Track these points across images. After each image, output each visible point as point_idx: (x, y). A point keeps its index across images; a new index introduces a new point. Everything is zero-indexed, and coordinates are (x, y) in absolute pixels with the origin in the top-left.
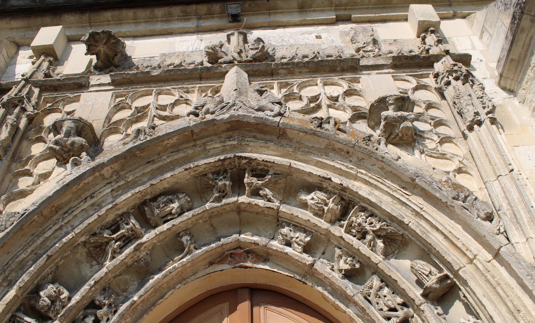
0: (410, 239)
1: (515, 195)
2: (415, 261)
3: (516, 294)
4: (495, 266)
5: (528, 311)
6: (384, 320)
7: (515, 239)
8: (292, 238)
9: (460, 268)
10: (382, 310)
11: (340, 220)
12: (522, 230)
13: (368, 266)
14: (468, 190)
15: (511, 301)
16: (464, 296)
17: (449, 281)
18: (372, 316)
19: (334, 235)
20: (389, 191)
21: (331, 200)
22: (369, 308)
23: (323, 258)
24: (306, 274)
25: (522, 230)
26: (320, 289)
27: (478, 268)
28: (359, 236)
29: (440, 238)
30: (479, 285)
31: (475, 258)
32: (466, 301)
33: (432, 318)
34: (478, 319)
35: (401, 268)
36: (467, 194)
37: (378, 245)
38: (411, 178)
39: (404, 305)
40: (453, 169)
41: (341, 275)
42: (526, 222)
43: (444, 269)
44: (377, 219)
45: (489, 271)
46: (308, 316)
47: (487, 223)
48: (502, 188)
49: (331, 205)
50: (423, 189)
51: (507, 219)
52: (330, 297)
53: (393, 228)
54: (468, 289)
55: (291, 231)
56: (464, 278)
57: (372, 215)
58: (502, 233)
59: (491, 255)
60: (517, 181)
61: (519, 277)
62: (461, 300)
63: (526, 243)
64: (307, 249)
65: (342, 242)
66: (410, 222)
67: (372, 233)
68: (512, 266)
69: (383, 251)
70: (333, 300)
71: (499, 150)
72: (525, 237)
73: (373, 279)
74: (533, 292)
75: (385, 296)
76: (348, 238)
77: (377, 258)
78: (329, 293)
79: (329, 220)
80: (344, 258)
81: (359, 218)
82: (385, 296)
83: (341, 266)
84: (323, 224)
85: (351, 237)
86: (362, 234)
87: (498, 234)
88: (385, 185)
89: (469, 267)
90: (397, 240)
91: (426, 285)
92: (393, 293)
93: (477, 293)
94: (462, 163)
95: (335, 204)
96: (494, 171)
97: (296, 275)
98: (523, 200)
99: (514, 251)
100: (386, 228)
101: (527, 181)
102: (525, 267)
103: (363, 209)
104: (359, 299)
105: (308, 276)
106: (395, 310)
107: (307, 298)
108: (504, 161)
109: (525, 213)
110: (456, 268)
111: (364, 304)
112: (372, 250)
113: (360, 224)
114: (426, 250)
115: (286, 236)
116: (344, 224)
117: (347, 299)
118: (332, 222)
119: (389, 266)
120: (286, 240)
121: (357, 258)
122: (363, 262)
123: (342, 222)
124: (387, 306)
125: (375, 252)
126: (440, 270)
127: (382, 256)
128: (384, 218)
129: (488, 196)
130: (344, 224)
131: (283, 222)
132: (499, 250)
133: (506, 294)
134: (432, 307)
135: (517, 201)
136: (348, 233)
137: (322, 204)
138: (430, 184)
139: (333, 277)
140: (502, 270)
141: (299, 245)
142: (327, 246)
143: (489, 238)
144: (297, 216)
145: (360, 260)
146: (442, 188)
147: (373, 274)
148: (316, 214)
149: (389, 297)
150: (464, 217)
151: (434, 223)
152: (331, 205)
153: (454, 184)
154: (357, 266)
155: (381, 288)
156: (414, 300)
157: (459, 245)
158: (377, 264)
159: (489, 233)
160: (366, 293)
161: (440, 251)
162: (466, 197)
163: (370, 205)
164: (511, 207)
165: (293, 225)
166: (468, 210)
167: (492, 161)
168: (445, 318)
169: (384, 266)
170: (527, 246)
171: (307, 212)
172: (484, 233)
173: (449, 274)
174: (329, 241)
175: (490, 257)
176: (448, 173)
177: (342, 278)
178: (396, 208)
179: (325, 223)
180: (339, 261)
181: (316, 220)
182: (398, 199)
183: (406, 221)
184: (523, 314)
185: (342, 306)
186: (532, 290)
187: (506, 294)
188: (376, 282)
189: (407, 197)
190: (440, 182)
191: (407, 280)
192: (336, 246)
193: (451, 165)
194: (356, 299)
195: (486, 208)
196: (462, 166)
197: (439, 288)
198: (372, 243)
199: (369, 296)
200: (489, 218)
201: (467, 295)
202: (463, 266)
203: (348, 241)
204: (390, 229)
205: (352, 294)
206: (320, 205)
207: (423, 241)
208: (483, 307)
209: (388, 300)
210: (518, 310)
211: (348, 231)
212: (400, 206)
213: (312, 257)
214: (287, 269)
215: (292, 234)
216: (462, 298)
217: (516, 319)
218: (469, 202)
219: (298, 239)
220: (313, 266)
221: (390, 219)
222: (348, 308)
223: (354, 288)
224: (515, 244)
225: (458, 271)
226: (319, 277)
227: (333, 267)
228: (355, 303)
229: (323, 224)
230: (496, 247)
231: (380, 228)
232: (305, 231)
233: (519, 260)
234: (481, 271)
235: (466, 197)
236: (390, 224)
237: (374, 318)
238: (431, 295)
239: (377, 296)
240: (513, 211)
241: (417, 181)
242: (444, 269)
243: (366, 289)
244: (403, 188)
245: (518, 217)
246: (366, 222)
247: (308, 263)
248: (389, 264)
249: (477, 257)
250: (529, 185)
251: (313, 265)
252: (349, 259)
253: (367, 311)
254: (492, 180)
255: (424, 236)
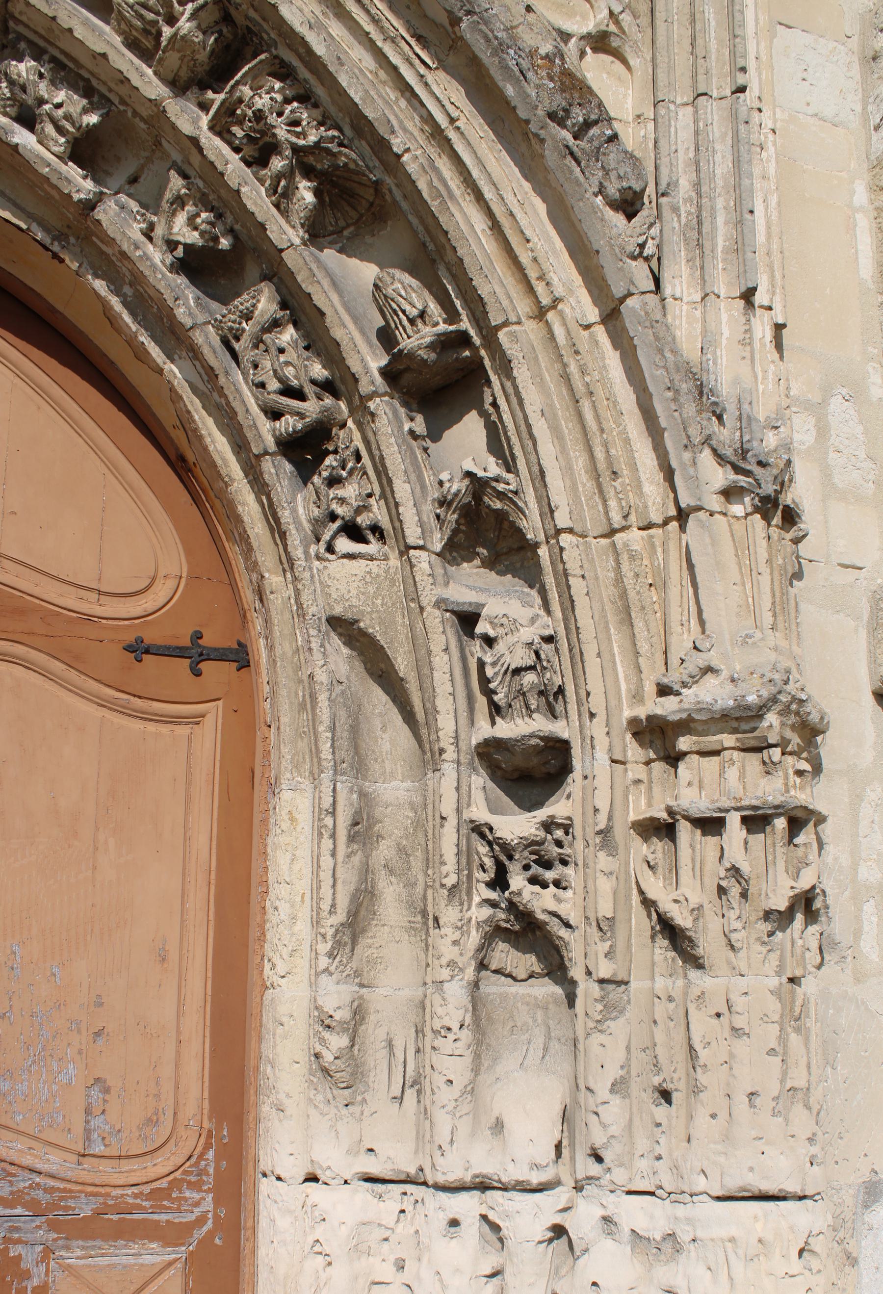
0: (395, 202)
1: (721, 165)
2: (392, 271)
3: (624, 432)
4: (597, 343)
5: (638, 480)
6: (262, 416)
7: (674, 286)
8: (41, 102)
9: (506, 324)
10: (262, 385)
11: (203, 86)
12: (702, 268)
13: (254, 250)
14: (600, 105)
15: (606, 445)
16: (494, 404)
17: (467, 353)
18: (231, 398)
19: (174, 127)
20: (376, 35)
21: (190, 7)
22: (227, 373)
23: (129, 195)
24: (66, 230)
25: (702, 268)
26: (100, 286)
27: (553, 338)
28: (248, 151)
29: (480, 223)
30: (541, 385)
31: (554, 307)
32: (494, 417)
33: (393, 440)
34: (509, 471)
35: (349, 283)
36: (593, 117)
37: (298, 195)
38: (450, 13)
39: (328, 387)
40: (584, 30)
41: (169, 259)
42: (720, 249)
43: (464, 317)
44: (317, 113)
45: (577, 352)
46: (54, 362)
47: (618, 219)
48: (697, 133)
49: (185, 25)
50: (474, 61)
51: (676, 225)
52: (127, 318)
53: (353, 155)
54: (508, 384)
55: (41, 76)
56: (508, 352)
57: (305, 98)
58: (647, 259)
59: (596, 311)
60: (742, 127)
61: (645, 389)
62: (483, 414)
63: (699, 306)
64: (84, 150)
65: (196, 159)
66: (407, 150)
67: (288, 152)
68: (639, 352)
69: (307, 218)
70: (134, 327)
71: (731, 15)
72: (703, 287)
73: (260, 292)
74: (666, 434)
75: (282, 351)
76: (216, 147)
77: (286, 234)
78: (125, 304)
79: (170, 77)
80: (190, 208)
81: (264, 97)
82: (282, 351)
83: (176, 230)
84: (148, 82)
85: (226, 150)
86: (261, 150)
87: (634, 258)
88: (367, 11)
89: (531, 329)
90: (361, 197)
91: (401, 347)
92: (307, 348)
93: (527, 403)
94: (617, 23)
95: (199, 27)
96: (694, 77)
97: (35, 227)
98: (737, 187)
99: (658, 316)
100: (336, 149)
101: (771, 136)
102: (671, 366)
103: (283, 72)
104: (207, 339)
105: (72, 240)
106: (298, 394)
107: (59, 307)
108: (733, 53)
109: (726, 223)
110: (495, 319)
111: (217, 357)
112: (277, 206)
113: (259, 116)
114: (431, 246)
115: (24, 89)
116: (213, 101)
117: (173, 333)
118: (178, 86)
119: (314, 266)
120: (22, 105)
121: (230, 219)
122: (244, 237)
123: (210, 94)
124: (280, 380)
125: (285, 213)
126: (452, 316)
127: (301, 232)
128: (338, 116)
129: (651, 145)
130: (213, 101)
131: (20, 37)
132: (622, 300)
133: (599, 423)
134: (402, 411)
135: (720, 183)
136: (219, 134)
137: (157, 13)
138: (500, 48)
139: (146, 257)
140: (613, 360)
141: (60, 130)
142: (149, 160)
143: (607, 261)
144: (70, 31)
145: (237, 227)
146: (530, 75)
147: (265, 278)
148: (132, 45)
149: (291, 355)
150: (562, 180)
151: (475, 173)
152: (185, 25)
153: (567, 74)
154: (225, 243)
155: (275, 324)
156: (356, 381)
157: (525, 259)
158: (282, 251)
159: (612, 246)
160: (231, 329)
161: (466, 261)
162: (588, 124)
163: (307, 65)
164: (699, 195)
165: (53, 60)
166: (579, 163)
167: (700, 42)
168: (426, 450)
169: (301, 261)
170: (698, 313)
171: (107, 29)
172: (599, 243)
173: (472, 332)
174: (157, 144)
175: (593, 314)
176: (566, 36)
177: (172, 268)
178: (380, 96)
179: (155, 80)
180: (174, 214)
181: (126, 62)
182: (395, 69)
183: (397, 144)
184: (622, 484)
185: (155, 352)
186: (665, 429)
187: (599, 423)
188: (265, 303)
189: (422, 70)
190: (533, 53)
191: (356, 319)
192: (175, 166)
193: (584, 17)
194: (198, 337)
195: (630, 175)
196: (612, 28)
197: (435, 362)
198: (283, 183)
199: (238, 339)
200: (629, 205)
201: (502, 402)
202: (514, 319)
203: (212, 158)
204: (346, 157)
205: (188, 322)
206: (151, 16)
207: (430, 220)
208: (530, 443)
209: (288, 363)
210: (614, 473)
211: (219, 128)
212: (392, 95)
213: (94, 180)
214: (9, 200)
215: (43, 89)
216: (487, 406)
217: (601, 492)
218: (591, 141)
219: (60, 112)
220: (93, 208)
221: (353, 127)
222: (172, 361)
223: (198, 304)
224: (669, 300)
225: (498, 328)
226: (104, 248)
227: (151, 227)
228: (193, 350)
229: (148, 82)
230: (618, 291)
231: (317, 144)
232: (87, 90)
233: (664, 342)
234: (557, 346)
235: (588, 124)
236: (351, 140)
237: (236, 405)
238: (406, 379)
239: (258, 342)
240: (699, 207)
241: (463, 25)
242: (464, 317)
243: (233, 317)
244: (419, 38)
245: (706, 228)
246: (280, 114)
247: (76, 197)
248: (318, 260)
249: (560, 307)
250: (771, 150)
251: (90, 206)
252: (204, 215)
253: (222, 380)
254: (679, 101)
255: (434, 205)
